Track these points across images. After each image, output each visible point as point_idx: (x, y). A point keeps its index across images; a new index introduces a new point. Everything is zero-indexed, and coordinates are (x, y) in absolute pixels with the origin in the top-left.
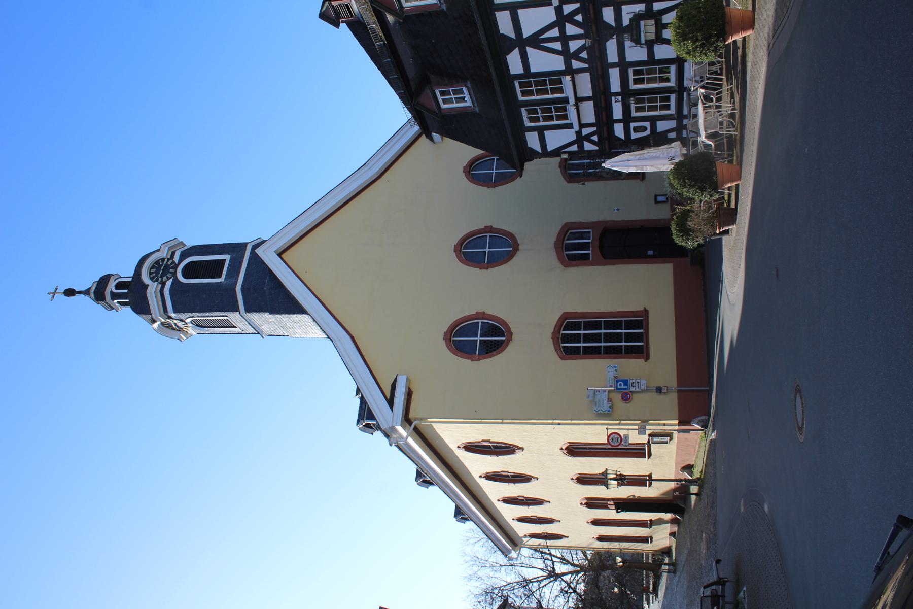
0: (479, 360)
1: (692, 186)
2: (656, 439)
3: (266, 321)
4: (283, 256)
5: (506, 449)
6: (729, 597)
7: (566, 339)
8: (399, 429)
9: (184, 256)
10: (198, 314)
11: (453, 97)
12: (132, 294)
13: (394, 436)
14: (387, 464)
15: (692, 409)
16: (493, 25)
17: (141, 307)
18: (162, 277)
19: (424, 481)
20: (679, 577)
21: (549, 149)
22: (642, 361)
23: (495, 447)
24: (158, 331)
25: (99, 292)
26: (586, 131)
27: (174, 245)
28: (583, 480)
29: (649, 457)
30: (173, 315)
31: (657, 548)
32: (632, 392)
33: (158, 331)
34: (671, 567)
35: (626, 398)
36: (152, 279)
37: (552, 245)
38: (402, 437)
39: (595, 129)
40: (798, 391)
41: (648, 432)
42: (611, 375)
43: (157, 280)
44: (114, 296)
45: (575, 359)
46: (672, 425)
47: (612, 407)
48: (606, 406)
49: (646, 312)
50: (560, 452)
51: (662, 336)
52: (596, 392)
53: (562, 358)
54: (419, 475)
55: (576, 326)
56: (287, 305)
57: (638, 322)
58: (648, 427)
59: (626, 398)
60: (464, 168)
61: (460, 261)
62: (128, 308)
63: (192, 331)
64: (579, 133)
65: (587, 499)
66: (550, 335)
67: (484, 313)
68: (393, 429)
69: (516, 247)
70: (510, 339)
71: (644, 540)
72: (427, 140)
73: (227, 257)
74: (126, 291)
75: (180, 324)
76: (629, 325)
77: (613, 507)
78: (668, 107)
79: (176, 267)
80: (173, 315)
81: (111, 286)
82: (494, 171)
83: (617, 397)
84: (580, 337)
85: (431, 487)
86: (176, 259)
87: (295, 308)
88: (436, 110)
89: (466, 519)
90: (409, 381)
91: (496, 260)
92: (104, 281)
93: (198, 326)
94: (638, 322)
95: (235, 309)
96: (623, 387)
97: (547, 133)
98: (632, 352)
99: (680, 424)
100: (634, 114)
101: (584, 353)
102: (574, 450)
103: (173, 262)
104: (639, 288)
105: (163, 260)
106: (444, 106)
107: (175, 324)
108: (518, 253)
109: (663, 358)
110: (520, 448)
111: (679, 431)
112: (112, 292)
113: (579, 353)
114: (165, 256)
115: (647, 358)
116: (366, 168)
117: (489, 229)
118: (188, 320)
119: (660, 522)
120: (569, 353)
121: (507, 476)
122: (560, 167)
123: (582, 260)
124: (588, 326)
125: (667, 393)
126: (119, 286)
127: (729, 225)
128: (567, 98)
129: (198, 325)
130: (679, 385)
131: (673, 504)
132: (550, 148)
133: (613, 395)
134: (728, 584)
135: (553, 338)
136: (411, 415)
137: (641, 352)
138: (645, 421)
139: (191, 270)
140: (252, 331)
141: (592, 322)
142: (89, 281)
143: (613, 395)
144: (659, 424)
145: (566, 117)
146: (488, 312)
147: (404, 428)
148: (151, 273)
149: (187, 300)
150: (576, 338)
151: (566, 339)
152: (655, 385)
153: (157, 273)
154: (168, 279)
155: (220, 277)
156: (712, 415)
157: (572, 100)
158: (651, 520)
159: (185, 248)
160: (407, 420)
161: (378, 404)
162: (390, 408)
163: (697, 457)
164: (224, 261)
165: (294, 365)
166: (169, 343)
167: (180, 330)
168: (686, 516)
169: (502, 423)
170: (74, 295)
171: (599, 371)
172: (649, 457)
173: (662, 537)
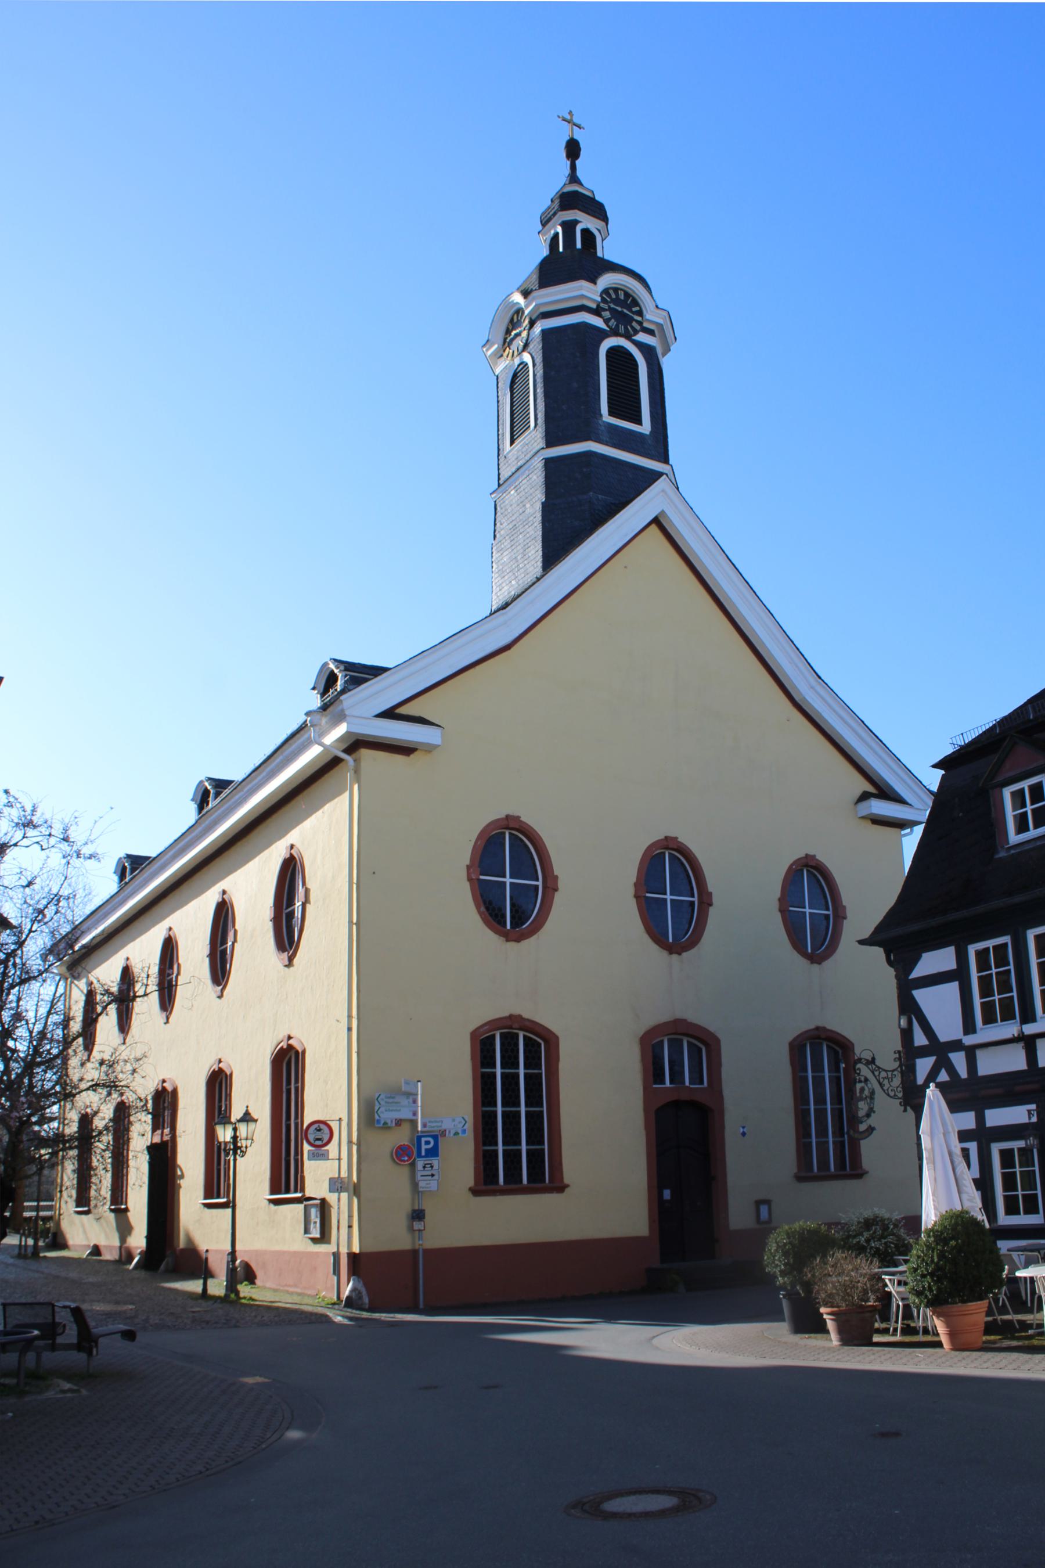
0: (470, 879)
1: (942, 1255)
2: (314, 1213)
3: (529, 497)
4: (654, 527)
5: (287, 934)
6: (51, 1359)
7: (510, 1042)
8: (341, 729)
9: (649, 352)
10: (540, 372)
11: (1029, 808)
12: (572, 258)
13: (324, 721)
14: (254, 714)
15: (376, 1274)
16: (936, 943)
17: (553, 270)
18: (610, 309)
19: (206, 794)
20: (13, 1265)
21: (917, 994)
22: (471, 1182)
23: (291, 915)
24: (506, 301)
25: (575, 199)
26: (958, 1060)
27: (664, 332)
28: (218, 1084)
29: (271, 1201)
30: (538, 329)
31: (65, 1225)
32: (413, 1165)
33: (506, 301)
34: (30, 1251)
35: (402, 1154)
36: (606, 291)
37: (679, 1015)
38: (323, 734)
39: (963, 1073)
40: (689, 1500)
41: (332, 1198)
42: (447, 1125)
43: (603, 300)
44: (569, 227)
45: (473, 1058)
46: (347, 1239)
47: (386, 1127)
48: (387, 1115)
49: (559, 1187)
50: (282, 1034)
51: (517, 1220)
52: (412, 1096)
53: (474, 1035)
54: (221, 785)
55: (532, 1061)
56: (559, 539)
57: (542, 1174)
58: (344, 1196)
59: (402, 1154)
60: (814, 856)
61: (649, 848)
62: (545, 252)
63: (504, 366)
64: (956, 1045)
65: (175, 1091)
66: (516, 1011)
67: (556, 890)
68: (341, 717)
69: (676, 948)
70: (508, 937)
71: (83, 1199)
72: (858, 793)
73: (646, 427)
74: (579, 245)
75: (519, 343)
76: (536, 1158)
77: (157, 1139)
78: (1011, 1208)
79: (628, 337)
80: (538, 329)
81: (586, 222)
82: (807, 910)
83: (402, 1137)
84: (514, 1064)
85: (193, 807)
86: (642, 337)
87: (554, 550)
88: (1000, 778)
89: (122, 876)
90: (429, 748)
91: (651, 913)
92: (598, 211)
93: (515, 376)
94: (542, 1174)
95: (551, 441)
96: (424, 1147)
97: (952, 988)
98: (486, 1163)
99: (353, 1257)
100: (996, 1148)
101: (483, 1075)
102: (287, 1065)
103: (636, 332)
104: (605, 1179)
105: (640, 313)
106: (1007, 793)
107: (518, 335)
108: (665, 953)
109: (472, 1221)
110: (291, 959)
111: (336, 1256)
112: (576, 222)
113: (483, 1065)
114: (648, 316)
115: (475, 1192)
116: (812, 679)
117: (706, 900)
118: (527, 357)
119: (124, 1229)
120: (482, 1047)
121: (224, 941)
122: (817, 1028)
123: (653, 1071)
124: (533, 1082)
125: (411, 1229)
126: (588, 236)
127: (841, 1331)
128: (974, 1031)
129: (517, 377)
130: (427, 1252)
131: (167, 1250)
132: (920, 995)
133: (406, 1128)
134: (83, 1356)
135: (511, 1017)
136: (365, 753)
137: (485, 1182)
138: (356, 1190)
139: (621, 364)
140: (505, 474)
141: (542, 1089)
142: (594, 180)
143: (406, 1128)
144: (350, 1217)
145: (989, 1018)
146: (558, 898)
147: (341, 739)
148: (616, 290)
149: (567, 355)
150: (510, 1060)
151: (510, 1042)
152: (428, 1206)
153: (617, 301)
154: (606, 321)
155: (611, 413)
156: (376, 1316)
157: (1029, 1029)
158: (126, 1210)
159: (660, 356)
160: (355, 744)
161: (362, 711)
162: (367, 724)
163: (275, 1290)
164: (639, 422)
165: (437, 552)
166: (483, 321)
167: (506, 343)
168: (142, 1274)
169: (350, 922)
170: (568, 156)
171: (448, 1100)
172: (271, 1201)
173: (86, 1232)
